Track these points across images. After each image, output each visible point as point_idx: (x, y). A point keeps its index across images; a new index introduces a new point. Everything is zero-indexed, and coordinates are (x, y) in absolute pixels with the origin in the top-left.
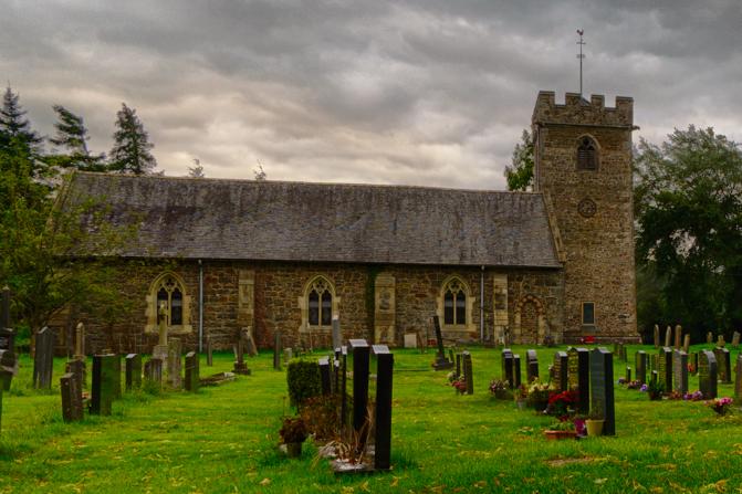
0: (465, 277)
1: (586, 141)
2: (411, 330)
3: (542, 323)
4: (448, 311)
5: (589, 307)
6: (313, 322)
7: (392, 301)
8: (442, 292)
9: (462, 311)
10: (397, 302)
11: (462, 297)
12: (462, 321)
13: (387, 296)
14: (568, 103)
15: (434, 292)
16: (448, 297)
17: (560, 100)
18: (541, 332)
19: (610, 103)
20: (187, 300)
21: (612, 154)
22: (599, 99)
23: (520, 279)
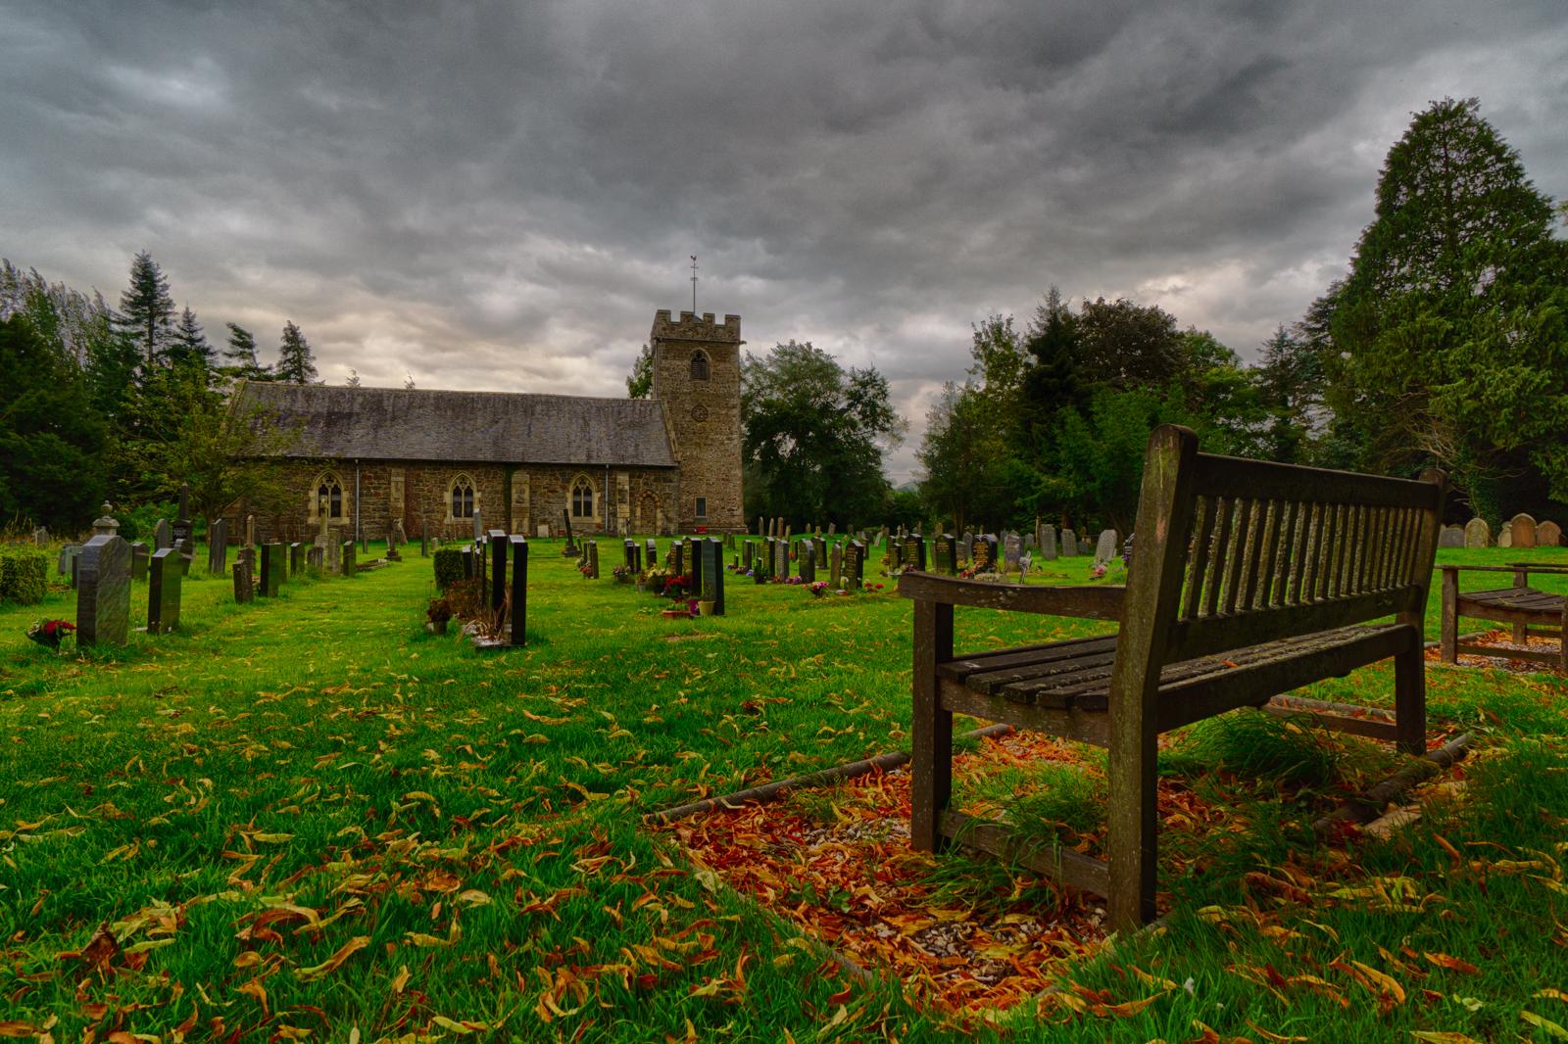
0: (592, 474)
1: (699, 354)
2: (544, 522)
4: (577, 505)
5: (701, 502)
6: (457, 514)
7: (526, 496)
8: (571, 488)
9: (588, 505)
11: (588, 493)
12: (589, 513)
13: (522, 492)
15: (565, 488)
16: (577, 492)
17: (676, 318)
20: (345, 495)
21: (721, 366)
22: (710, 317)
23: (640, 477)
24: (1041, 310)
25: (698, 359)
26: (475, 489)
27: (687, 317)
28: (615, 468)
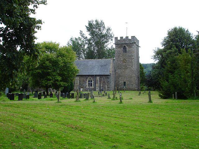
0: (92, 77)
1: (125, 46)
2: (82, 88)
3: (106, 86)
4: (89, 84)
5: (125, 83)
6: (89, 86)
7: (78, 82)
8: (88, 80)
9: (91, 84)
10: (79, 82)
11: (91, 81)
12: (91, 86)
13: (77, 81)
14: (132, 39)
15: (86, 80)
16: (89, 81)
17: (119, 39)
18: (106, 88)
19: (130, 38)
20: (93, 82)
21: (130, 49)
22: (127, 37)
23: (102, 77)
24: (58, 45)
25: (125, 48)
26: (92, 80)
27: (122, 38)
28: (96, 76)
